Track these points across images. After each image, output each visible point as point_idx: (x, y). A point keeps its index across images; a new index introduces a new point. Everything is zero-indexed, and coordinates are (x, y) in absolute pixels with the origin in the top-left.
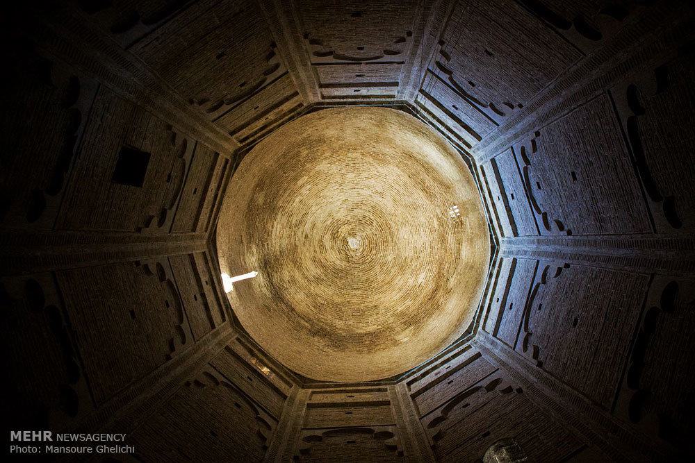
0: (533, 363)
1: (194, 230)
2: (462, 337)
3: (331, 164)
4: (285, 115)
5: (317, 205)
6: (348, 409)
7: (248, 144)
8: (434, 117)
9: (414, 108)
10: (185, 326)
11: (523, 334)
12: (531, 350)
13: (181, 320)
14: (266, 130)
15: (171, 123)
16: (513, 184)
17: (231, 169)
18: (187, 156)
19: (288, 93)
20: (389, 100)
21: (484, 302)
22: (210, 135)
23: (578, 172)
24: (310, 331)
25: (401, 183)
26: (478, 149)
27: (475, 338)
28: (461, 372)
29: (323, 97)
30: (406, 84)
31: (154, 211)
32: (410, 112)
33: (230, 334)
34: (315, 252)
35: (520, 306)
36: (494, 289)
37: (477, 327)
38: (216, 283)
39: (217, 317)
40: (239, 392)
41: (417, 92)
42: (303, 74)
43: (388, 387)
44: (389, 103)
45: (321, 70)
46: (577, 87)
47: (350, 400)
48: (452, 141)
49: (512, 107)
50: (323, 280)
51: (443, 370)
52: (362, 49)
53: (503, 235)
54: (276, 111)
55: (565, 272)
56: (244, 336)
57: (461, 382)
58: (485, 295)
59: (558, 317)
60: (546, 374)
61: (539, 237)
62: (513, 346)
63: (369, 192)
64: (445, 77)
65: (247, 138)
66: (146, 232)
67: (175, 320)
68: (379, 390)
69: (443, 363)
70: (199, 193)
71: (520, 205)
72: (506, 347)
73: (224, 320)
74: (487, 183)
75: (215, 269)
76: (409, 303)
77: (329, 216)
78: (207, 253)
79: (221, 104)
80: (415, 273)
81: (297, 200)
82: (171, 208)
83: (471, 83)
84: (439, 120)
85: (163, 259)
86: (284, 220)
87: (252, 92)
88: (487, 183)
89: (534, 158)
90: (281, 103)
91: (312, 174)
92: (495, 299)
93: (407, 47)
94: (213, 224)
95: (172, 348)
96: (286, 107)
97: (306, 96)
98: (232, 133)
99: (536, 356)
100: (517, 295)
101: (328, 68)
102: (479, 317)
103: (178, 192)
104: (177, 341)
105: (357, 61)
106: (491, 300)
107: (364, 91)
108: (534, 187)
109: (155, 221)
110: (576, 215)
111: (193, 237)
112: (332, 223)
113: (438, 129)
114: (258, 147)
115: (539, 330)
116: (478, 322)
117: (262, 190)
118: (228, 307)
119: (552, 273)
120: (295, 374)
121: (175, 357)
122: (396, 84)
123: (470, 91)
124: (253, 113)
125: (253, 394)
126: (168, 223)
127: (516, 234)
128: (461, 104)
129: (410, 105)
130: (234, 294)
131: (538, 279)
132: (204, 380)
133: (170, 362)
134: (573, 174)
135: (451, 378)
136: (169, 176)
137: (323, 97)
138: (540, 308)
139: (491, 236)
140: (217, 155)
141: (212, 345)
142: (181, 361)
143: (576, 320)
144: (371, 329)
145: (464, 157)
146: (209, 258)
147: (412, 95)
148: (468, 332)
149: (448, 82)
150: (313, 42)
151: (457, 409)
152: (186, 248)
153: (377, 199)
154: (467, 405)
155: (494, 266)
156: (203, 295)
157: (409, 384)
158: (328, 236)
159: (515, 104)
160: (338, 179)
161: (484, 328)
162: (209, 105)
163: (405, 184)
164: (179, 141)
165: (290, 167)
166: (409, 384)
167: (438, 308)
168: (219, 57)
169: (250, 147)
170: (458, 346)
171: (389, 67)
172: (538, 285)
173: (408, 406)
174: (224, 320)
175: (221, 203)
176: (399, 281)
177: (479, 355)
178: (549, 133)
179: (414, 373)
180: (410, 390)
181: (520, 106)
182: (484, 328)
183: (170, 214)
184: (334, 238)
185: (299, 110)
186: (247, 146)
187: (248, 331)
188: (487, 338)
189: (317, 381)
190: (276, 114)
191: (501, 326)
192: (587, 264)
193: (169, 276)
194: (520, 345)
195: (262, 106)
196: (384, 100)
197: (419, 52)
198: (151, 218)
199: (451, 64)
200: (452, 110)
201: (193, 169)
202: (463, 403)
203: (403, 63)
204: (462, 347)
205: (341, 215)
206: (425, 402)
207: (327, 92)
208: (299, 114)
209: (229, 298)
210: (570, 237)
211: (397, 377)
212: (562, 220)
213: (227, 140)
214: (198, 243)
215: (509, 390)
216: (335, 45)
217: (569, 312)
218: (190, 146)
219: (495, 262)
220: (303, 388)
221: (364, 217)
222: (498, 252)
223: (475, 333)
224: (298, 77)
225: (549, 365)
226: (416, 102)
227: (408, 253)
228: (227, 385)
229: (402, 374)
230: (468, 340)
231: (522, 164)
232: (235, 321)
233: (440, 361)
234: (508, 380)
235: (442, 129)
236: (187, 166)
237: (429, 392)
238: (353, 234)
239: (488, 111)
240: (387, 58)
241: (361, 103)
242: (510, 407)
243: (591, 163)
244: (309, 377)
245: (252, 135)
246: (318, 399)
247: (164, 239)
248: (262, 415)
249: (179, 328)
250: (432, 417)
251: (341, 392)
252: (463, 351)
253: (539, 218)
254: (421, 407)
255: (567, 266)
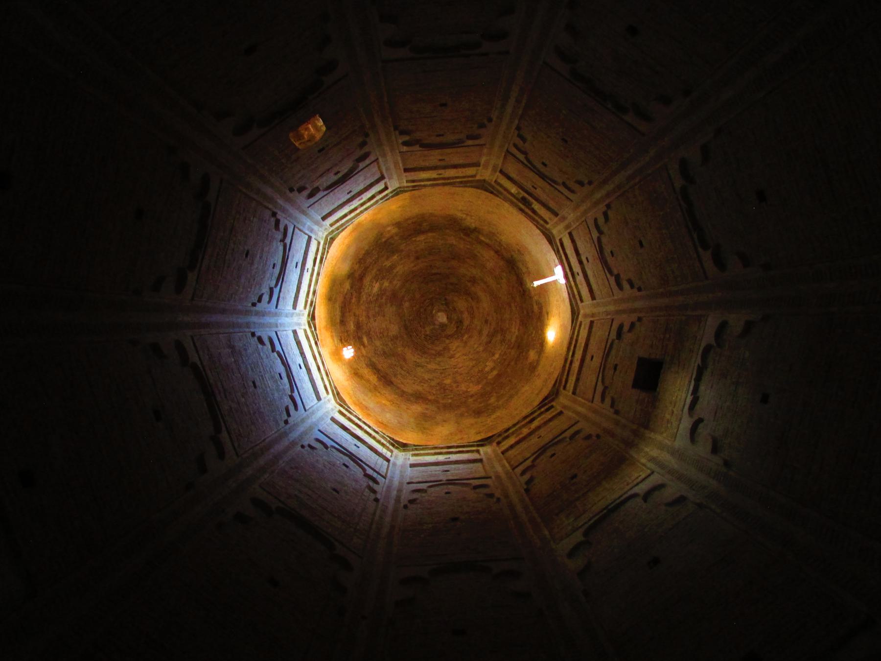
0: (280, 215)
1: (592, 322)
2: (339, 234)
3: (467, 392)
4: (513, 433)
5: (478, 352)
6: (443, 163)
7: (546, 404)
8: (374, 438)
9: (393, 446)
10: (595, 234)
11: (288, 241)
12: (282, 227)
13: (599, 239)
14: (529, 418)
15: (615, 416)
16: (301, 376)
17: (561, 380)
18: (600, 388)
19: (510, 452)
20: (417, 452)
21: (320, 268)
22: (580, 409)
23: (252, 389)
24: (479, 232)
25: (399, 376)
26: (332, 410)
27: (326, 233)
28: (340, 202)
29: (478, 451)
30: (403, 466)
31: (627, 337)
32: (397, 442)
33: (554, 227)
34: (478, 308)
35: (291, 265)
36: (311, 281)
37: (325, 244)
38: (569, 274)
39: (567, 242)
40: (543, 176)
41: (392, 459)
42: (499, 469)
43: (405, 184)
44: (416, 449)
45: (483, 474)
46: (262, 461)
47: (440, 172)
48: (356, 416)
49: (310, 446)
50: (469, 281)
51: (355, 203)
52: (447, 493)
53: (305, 331)
54: (521, 436)
55: (255, 300)
56: (542, 225)
57: (341, 195)
58: (318, 274)
59: (261, 258)
60: (270, 206)
61: (276, 329)
62: (296, 230)
63: (429, 366)
64: (370, 472)
65: (547, 410)
66: (634, 317)
67: (604, 240)
68: (413, 181)
69: (355, 209)
70: (588, 358)
71: (295, 360)
72: (301, 228)
73: (561, 240)
74: (322, 379)
75: (571, 287)
76: (388, 264)
77: (466, 343)
78: (579, 302)
79: (572, 437)
80: (382, 292)
81: (497, 356)
82: (613, 341)
83: (347, 467)
84: (370, 435)
85: (618, 295)
86: (508, 337)
87: (543, 449)
88: (322, 379)
89: (287, 401)
90: (517, 443)
91: (485, 381)
92: (310, 270)
93: (406, 496)
94: (574, 329)
95: (605, 214)
96: (512, 440)
97: (494, 451)
98: (561, 413)
99: (277, 222)
100: (292, 275)
101: (477, 475)
102: (323, 254)
103: (607, 355)
104: (601, 221)
105: (450, 482)
106: (313, 270)
107: (441, 458)
108: (284, 375)
109: (626, 328)
110: (250, 351)
111: (593, 315)
112: (463, 336)
113: (369, 427)
114: (536, 403)
115: (274, 244)
116: (324, 249)
117: (530, 364)
118: (557, 252)
119: (266, 298)
120: (492, 193)
121: (602, 207)
122: (412, 466)
123: (346, 459)
124: (542, 432)
125: (531, 175)
126: (615, 326)
127: (295, 332)
128: (352, 449)
129: (397, 448)
130: (552, 264)
131: (276, 291)
132: (576, 187)
133: (607, 202)
134: (255, 386)
135: (349, 196)
136: (615, 369)
137: (478, 451)
138: (274, 265)
139: (315, 329)
140: (574, 393)
141: (571, 217)
142: (597, 203)
143: (247, 255)
144: (422, 238)
145: (344, 402)
146: (577, 297)
147: (396, 457)
148: (333, 239)
149: (366, 467)
150: (491, 496)
151: (344, 170)
152: (598, 305)
153: (422, 361)
154: (336, 174)
155: (312, 302)
156: (581, 262)
157: (386, 188)
158: (466, 323)
159: (307, 448)
160: (459, 378)
161: (319, 243)
162: (582, 435)
163: (395, 375)
164: (608, 400)
165: (417, 495)
166: (386, 188)
167: (361, 259)
168: (574, 476)
169: (542, 404)
170: (342, 225)
171: (420, 480)
172: (276, 285)
173: (388, 169)
174: (561, 240)
175: (569, 348)
176: (397, 283)
177: (324, 218)
178: (277, 422)
179: (381, 199)
180: (385, 184)
181: (303, 447)
182: (319, 243)
183: (613, 335)
184: (460, 322)
185: (500, 439)
186: (547, 402)
187: (538, 231)
188: (316, 234)
189: (472, 187)
190: (521, 433)
191: (304, 246)
192: (240, 307)
193: (612, 280)
194: (290, 230)
195: (534, 440)
196: (422, 452)
197: (395, 492)
198: (630, 331)
199: (364, 482)
200: (359, 444)
201: (594, 379)
202: (340, 175)
203: (409, 483)
204: (338, 224)
205: (455, 345)
206: (372, 174)
207: (475, 456)
208: (500, 435)
209: (557, 261)
210: (252, 330)
211: (397, 194)
212: (260, 346)
213: (565, 407)
214: (588, 311)
215: (301, 190)
216: (472, 495)
217: (252, 264)
218: (598, 397)
219: (311, 305)
220: (484, 180)
221: (433, 343)
222: (309, 315)
223: (327, 237)
224: (503, 466)
225: (268, 213)
226: (392, 451)
227: (390, 310)
228: (555, 182)
229: (392, 197)
230: (333, 231)
231: (296, 394)
232: (550, 240)
233: (358, 211)
234: (301, 199)
235: (366, 428)
236: (600, 379)
237: (368, 182)
238: (443, 326)
239: (329, 443)
240: (424, 486)
241: (442, 448)
242: (299, 175)
243: (243, 397)
244: (479, 191)
245: (542, 413)
246: (470, 171)
247: (618, 312)
248: (521, 157)
249: (601, 232)
250: (367, 162)
251: (448, 178)
252: (337, 221)
253: (278, 348)
254: (376, 168)
255: (254, 305)
